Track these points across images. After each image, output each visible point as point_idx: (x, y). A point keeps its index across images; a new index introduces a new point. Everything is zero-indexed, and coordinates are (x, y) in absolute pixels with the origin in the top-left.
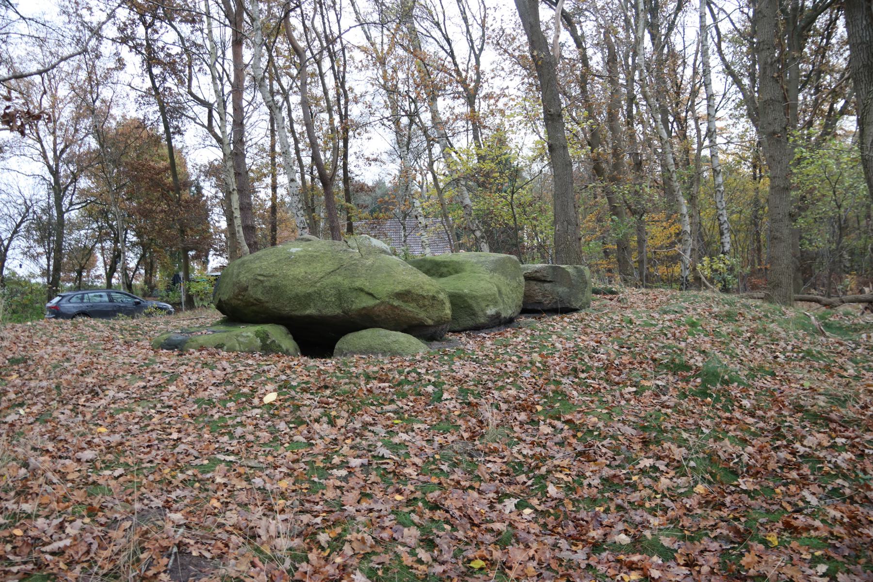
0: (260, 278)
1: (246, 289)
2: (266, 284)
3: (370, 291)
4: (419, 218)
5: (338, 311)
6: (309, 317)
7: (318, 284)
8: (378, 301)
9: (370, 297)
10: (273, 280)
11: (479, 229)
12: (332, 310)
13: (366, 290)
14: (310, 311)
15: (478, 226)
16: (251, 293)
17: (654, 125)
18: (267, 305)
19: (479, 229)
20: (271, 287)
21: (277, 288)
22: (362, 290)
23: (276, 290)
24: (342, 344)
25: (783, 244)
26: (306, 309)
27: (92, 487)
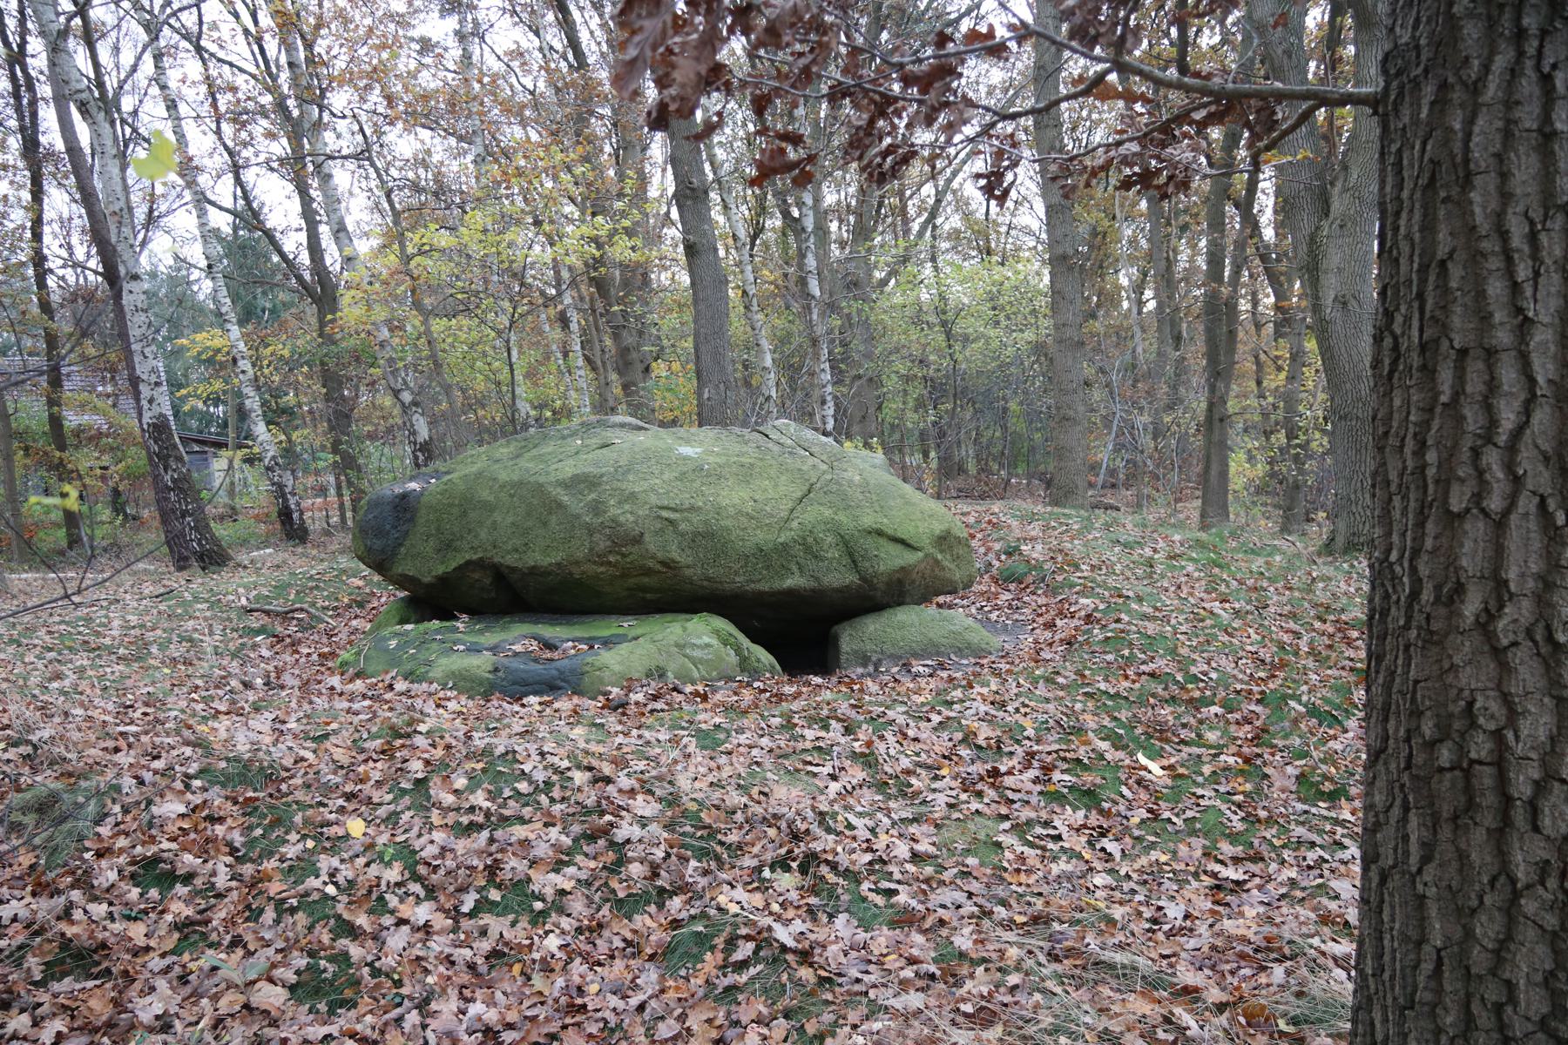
0: (665, 514)
1: (638, 540)
2: (683, 527)
3: (899, 535)
4: (241, 363)
5: (849, 578)
6: (791, 593)
7: (795, 524)
8: (920, 554)
9: (899, 547)
10: (695, 518)
11: (408, 388)
12: (838, 577)
13: (890, 532)
14: (793, 581)
15: (405, 383)
16: (652, 547)
17: (296, 113)
18: (688, 572)
19: (408, 388)
20: (697, 534)
21: (709, 535)
22: (880, 533)
23: (708, 539)
24: (853, 638)
25: (1079, 428)
26: (782, 577)
27: (252, 976)
